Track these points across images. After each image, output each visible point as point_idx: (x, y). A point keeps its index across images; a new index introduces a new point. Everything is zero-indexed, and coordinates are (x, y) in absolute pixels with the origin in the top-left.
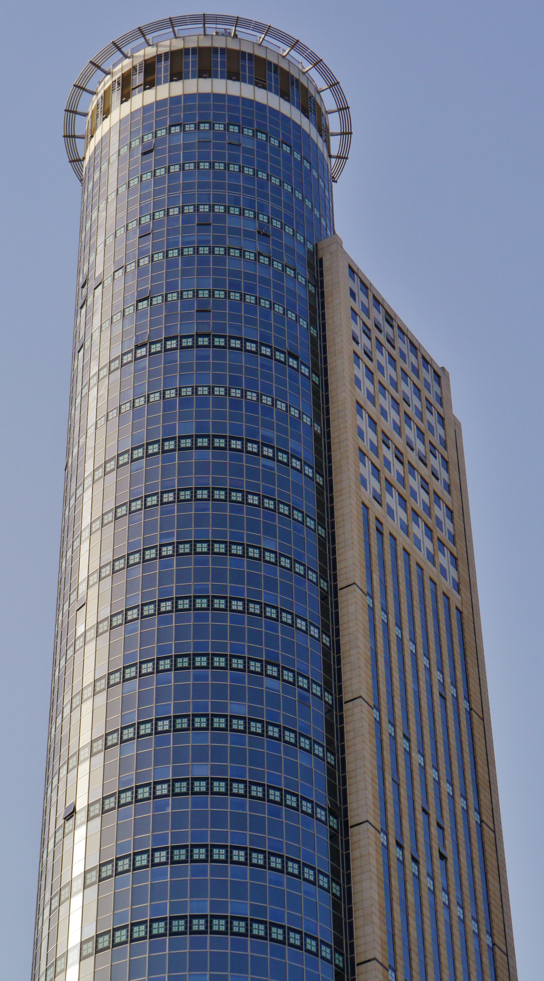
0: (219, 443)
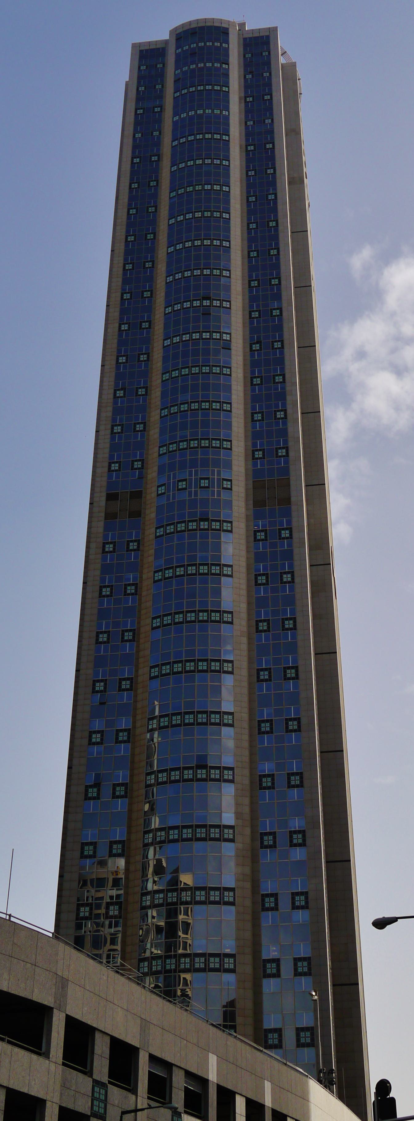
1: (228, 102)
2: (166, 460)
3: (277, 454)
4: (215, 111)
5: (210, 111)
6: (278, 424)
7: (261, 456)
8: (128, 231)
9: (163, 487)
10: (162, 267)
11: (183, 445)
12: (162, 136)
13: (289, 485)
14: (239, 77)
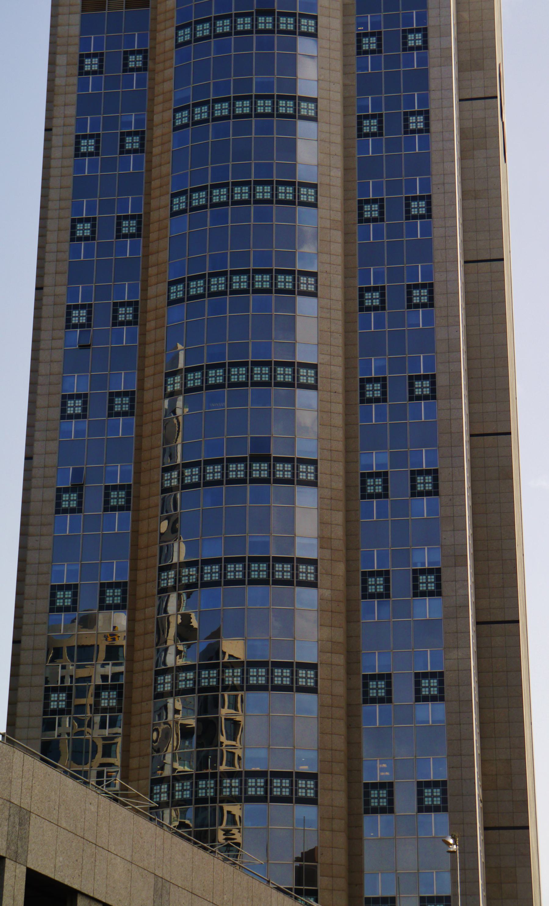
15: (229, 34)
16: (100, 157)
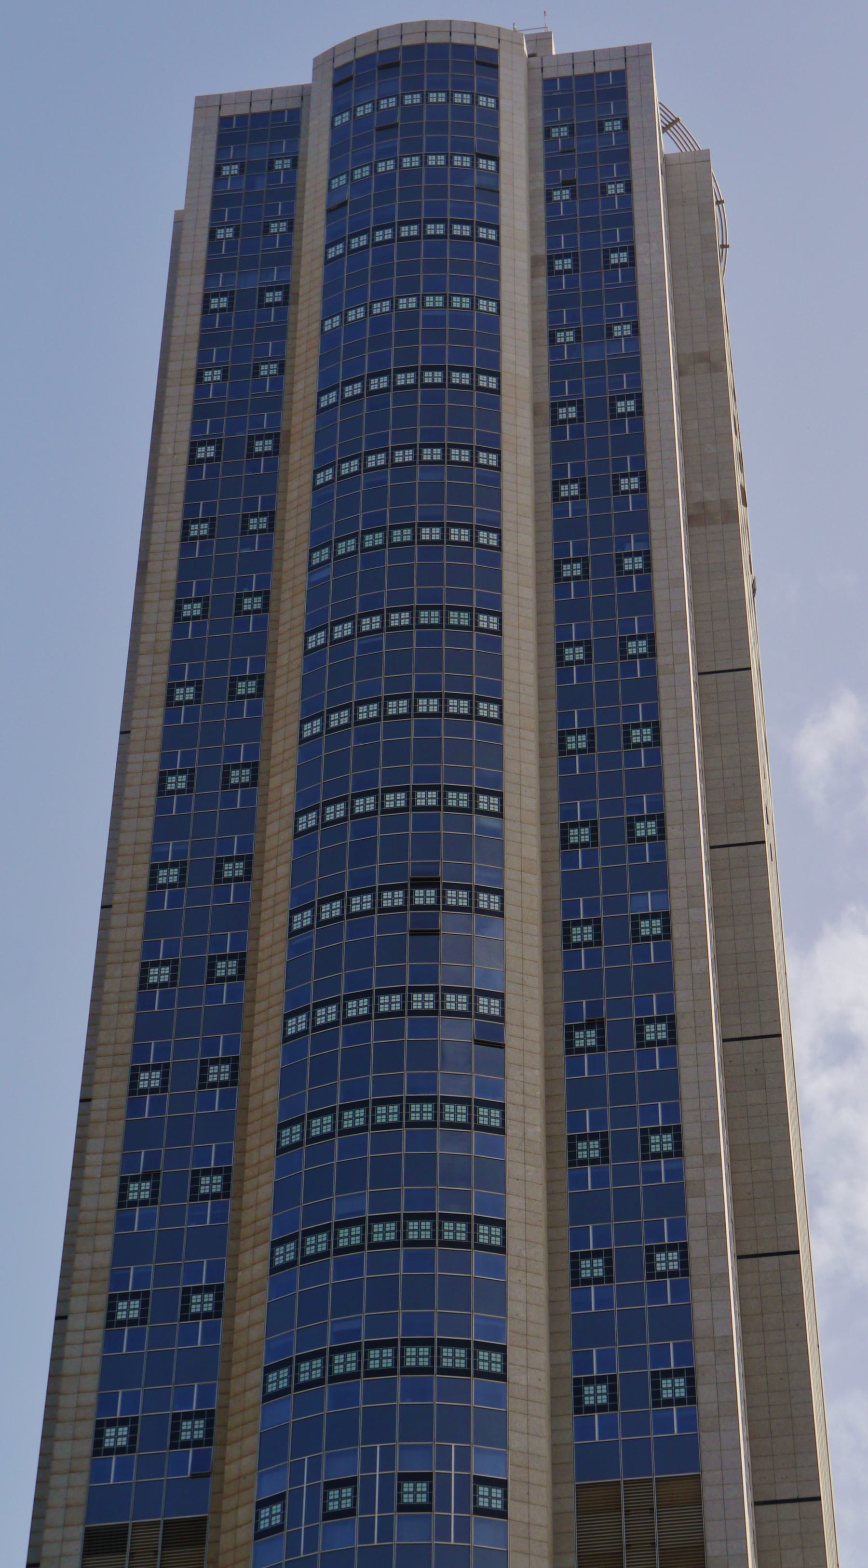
0: (457, 898)
1: (496, 272)
2: (287, 1412)
3: (657, 1394)
4: (456, 302)
5: (439, 301)
6: (657, 1293)
7: (603, 1400)
8: (175, 672)
9: (277, 1508)
10: (282, 785)
11: (350, 1237)
12: (286, 379)
13: (697, 1500)
14: (531, 196)
15: (355, 1375)
16: (135, 1455)
